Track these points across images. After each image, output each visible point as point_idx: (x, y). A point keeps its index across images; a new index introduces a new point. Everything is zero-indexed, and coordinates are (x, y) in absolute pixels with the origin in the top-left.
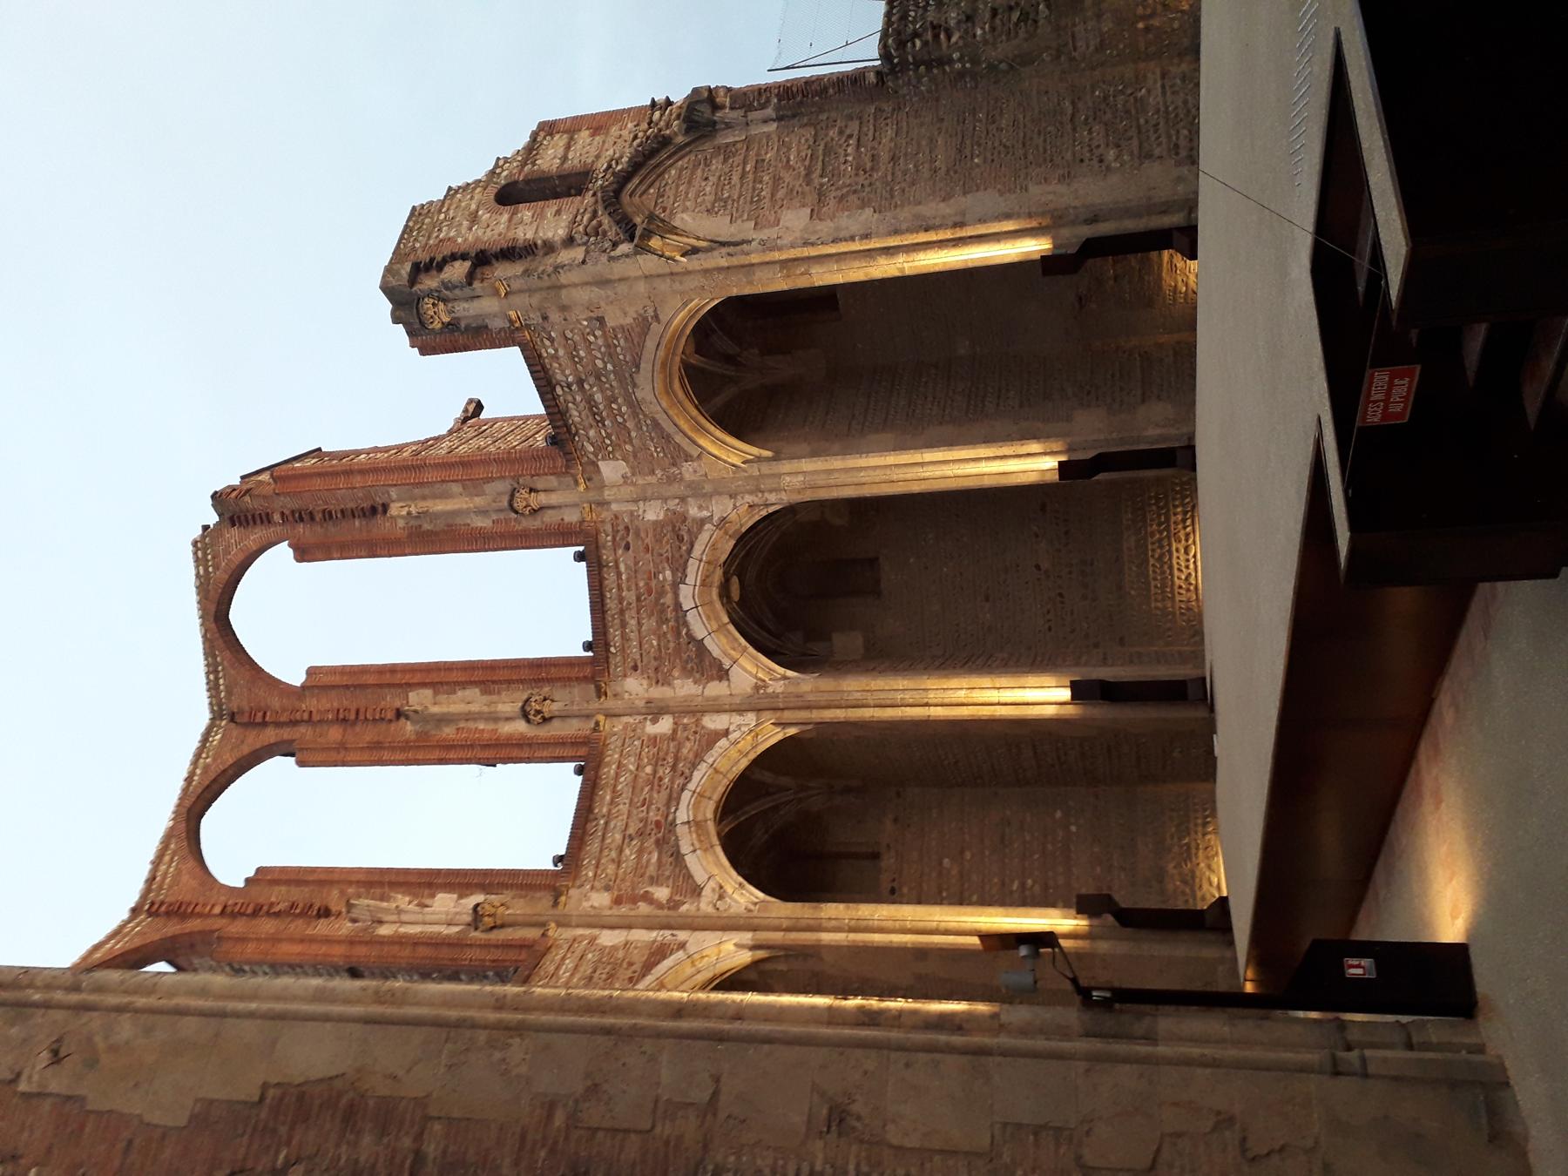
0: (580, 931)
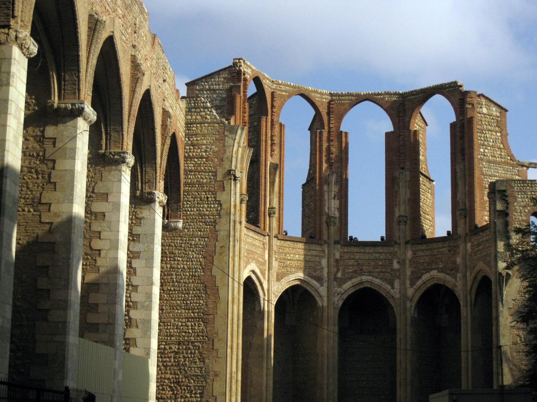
0: (326, 252)
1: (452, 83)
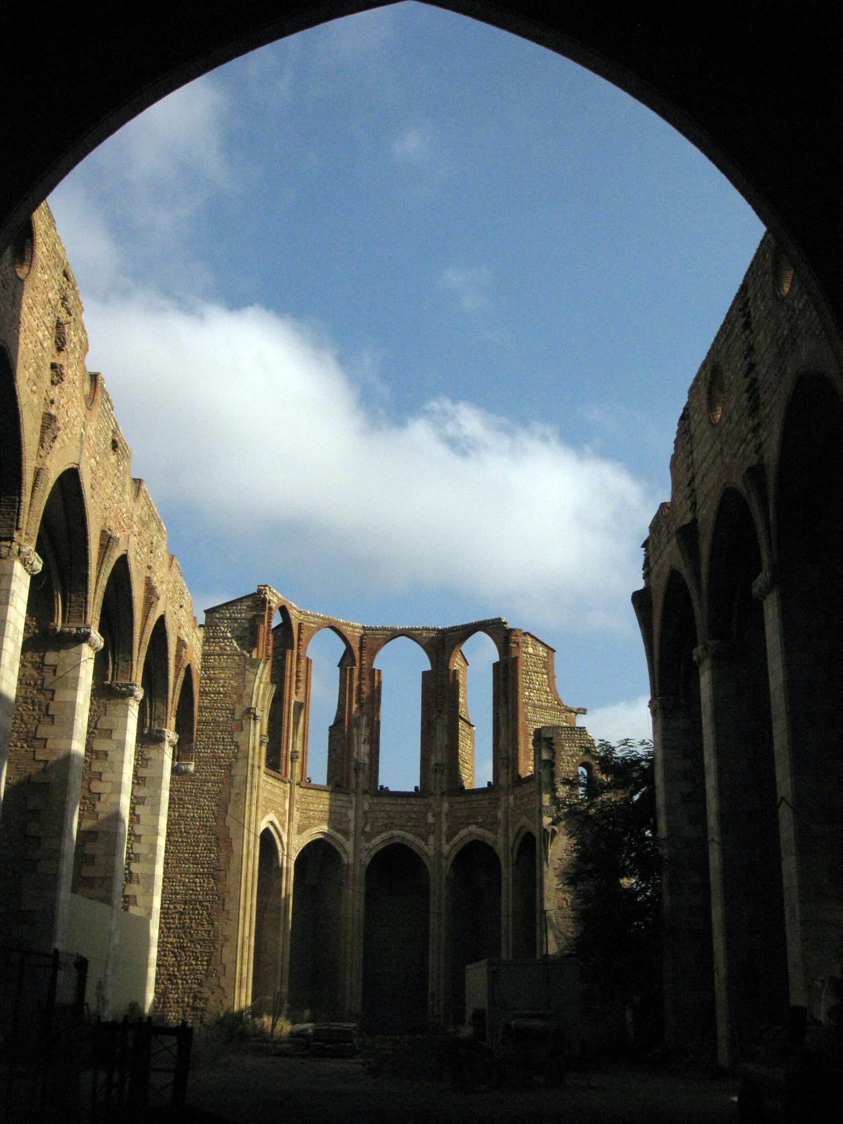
0: (354, 802)
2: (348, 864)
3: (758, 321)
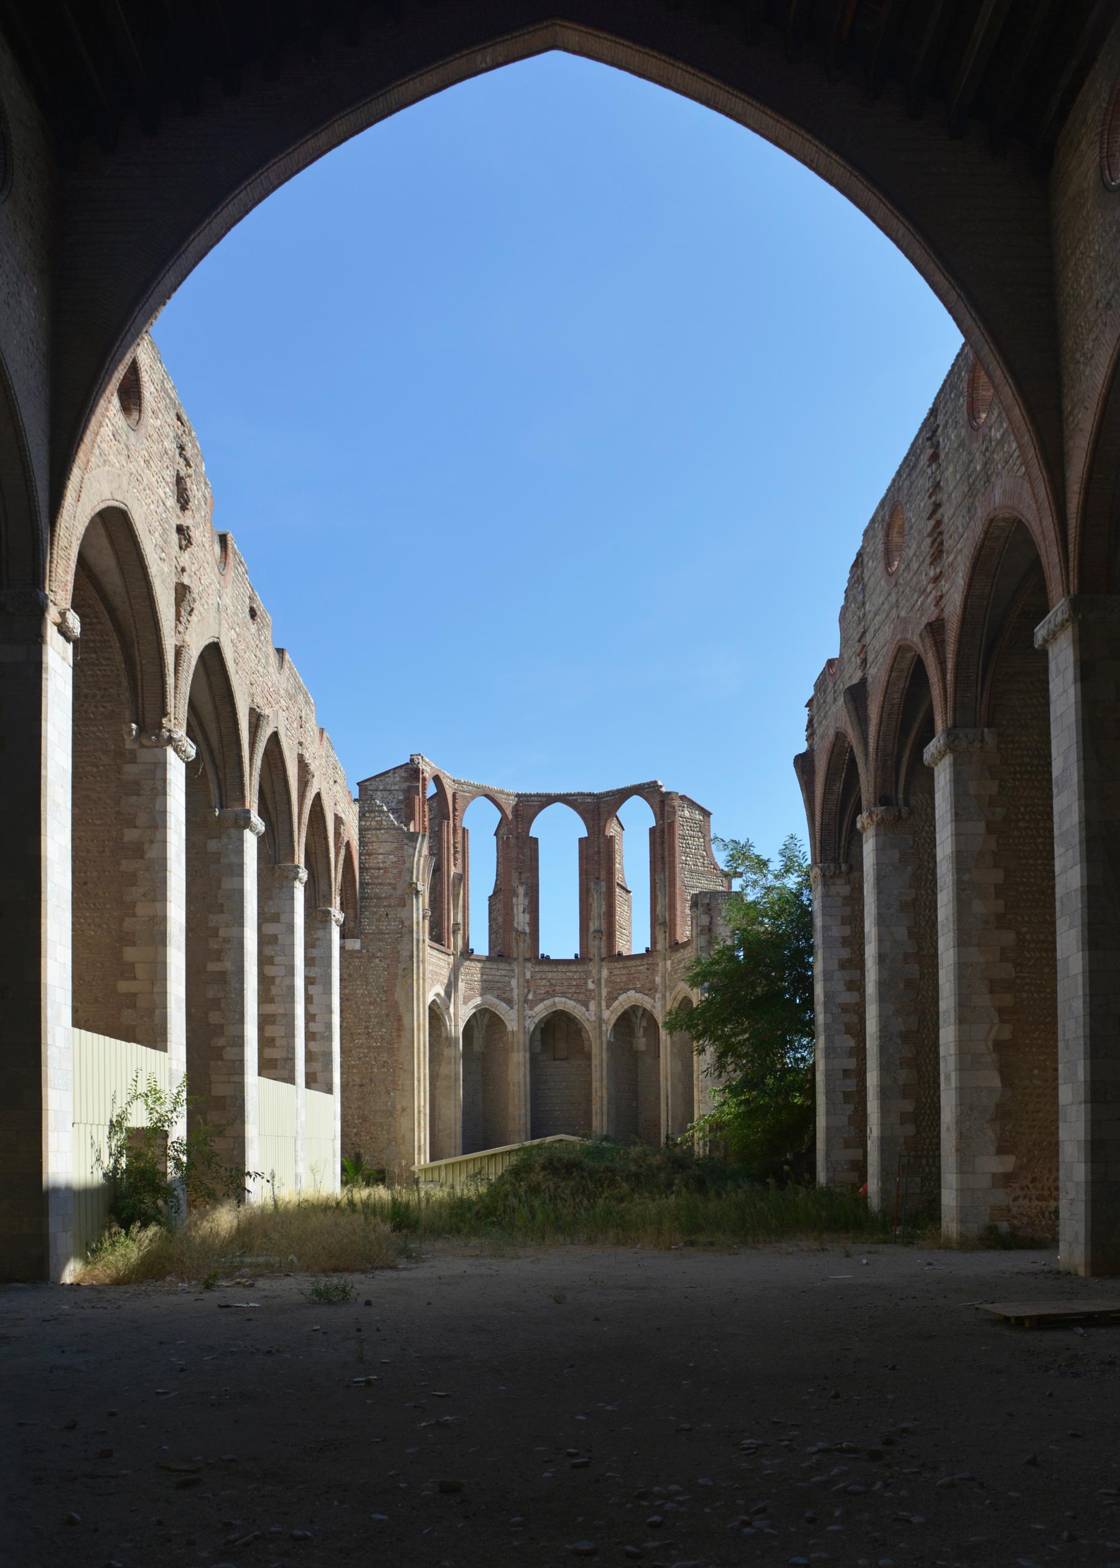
1: (652, 782)
2: (513, 1031)
3: (947, 453)
